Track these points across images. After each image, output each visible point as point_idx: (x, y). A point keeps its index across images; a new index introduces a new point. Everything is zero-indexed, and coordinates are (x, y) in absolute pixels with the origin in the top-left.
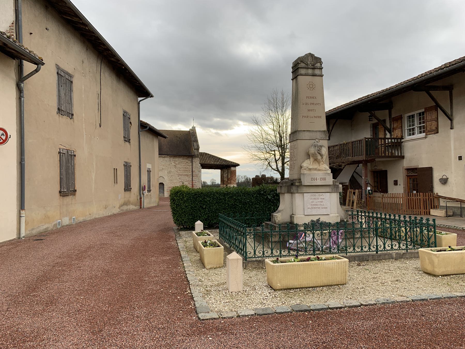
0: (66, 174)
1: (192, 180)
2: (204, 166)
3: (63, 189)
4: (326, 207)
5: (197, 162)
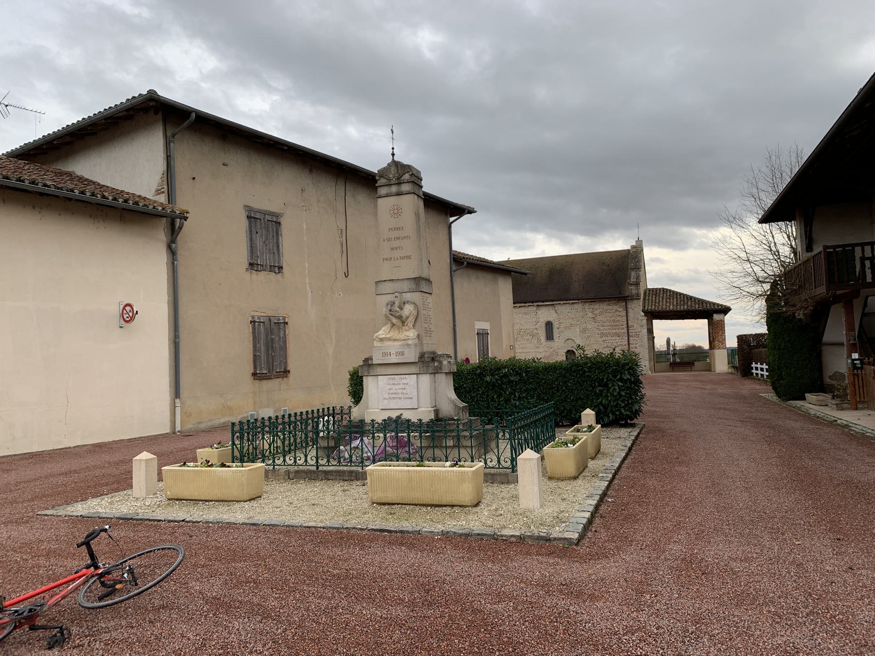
0: (268, 350)
1: (629, 344)
2: (653, 315)
3: (261, 369)
4: (411, 396)
5: (636, 310)
